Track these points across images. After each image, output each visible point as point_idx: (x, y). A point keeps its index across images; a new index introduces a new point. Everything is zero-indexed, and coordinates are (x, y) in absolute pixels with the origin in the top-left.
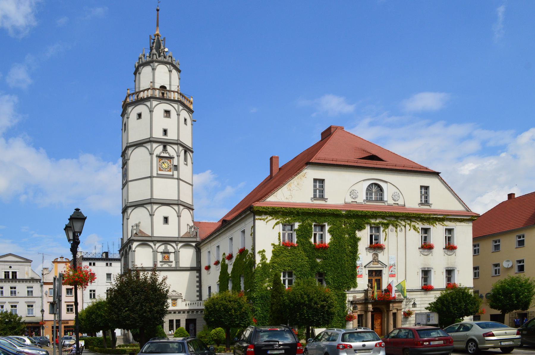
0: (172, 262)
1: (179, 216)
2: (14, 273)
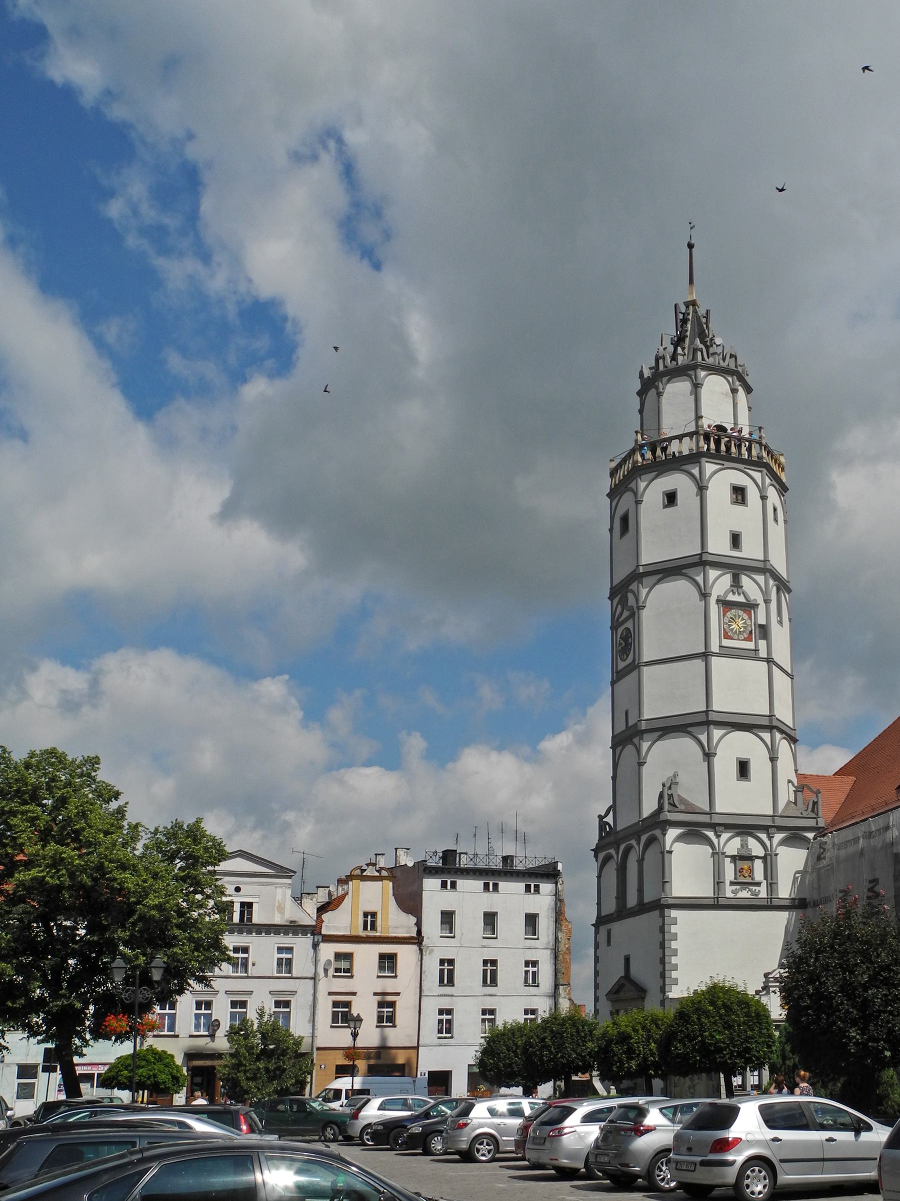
0: (758, 884)
1: (773, 759)
2: (247, 907)
